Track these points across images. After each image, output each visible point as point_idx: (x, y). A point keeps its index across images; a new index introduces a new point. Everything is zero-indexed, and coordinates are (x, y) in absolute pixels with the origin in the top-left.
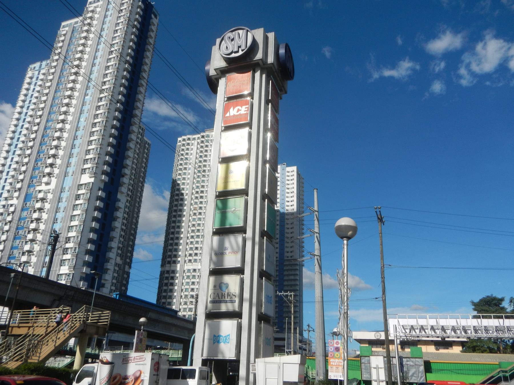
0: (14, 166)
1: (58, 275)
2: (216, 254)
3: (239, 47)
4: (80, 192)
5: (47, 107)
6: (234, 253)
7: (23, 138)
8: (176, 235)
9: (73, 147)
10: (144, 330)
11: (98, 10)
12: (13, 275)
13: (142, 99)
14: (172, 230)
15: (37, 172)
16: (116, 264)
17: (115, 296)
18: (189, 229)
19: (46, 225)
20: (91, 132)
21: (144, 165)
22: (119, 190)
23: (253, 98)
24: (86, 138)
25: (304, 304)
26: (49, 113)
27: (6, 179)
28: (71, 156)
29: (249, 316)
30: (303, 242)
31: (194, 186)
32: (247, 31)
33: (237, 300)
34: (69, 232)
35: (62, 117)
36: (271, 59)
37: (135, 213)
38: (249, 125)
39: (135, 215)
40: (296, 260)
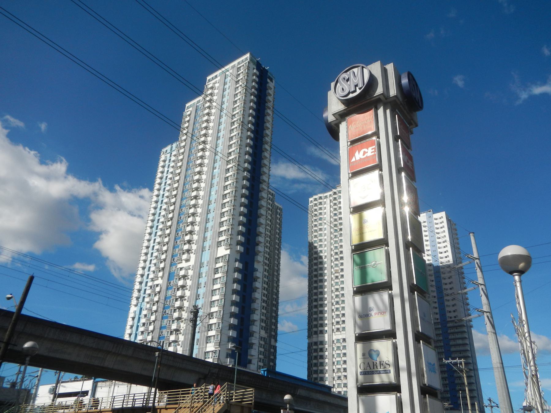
0: (157, 247)
1: (205, 353)
2: (360, 317)
3: (356, 86)
4: (218, 265)
5: (180, 186)
6: (381, 314)
7: (162, 219)
8: (320, 303)
9: (207, 221)
10: (290, 410)
11: (217, 85)
12: (157, 353)
13: (267, 163)
14: (315, 297)
15: (177, 250)
16: (261, 338)
17: (263, 372)
18: (333, 294)
19: (190, 302)
20: (222, 204)
21: (277, 231)
22: (255, 259)
23: (379, 137)
24: (219, 210)
25: (480, 373)
26: (183, 192)
27: (151, 260)
28: (206, 230)
29: (409, 388)
30: (467, 299)
31: (332, 247)
32: (363, 67)
33: (392, 369)
34: (211, 307)
35: (194, 194)
36: (393, 92)
37: (275, 282)
38: (379, 167)
39: (275, 285)
40: (461, 320)
